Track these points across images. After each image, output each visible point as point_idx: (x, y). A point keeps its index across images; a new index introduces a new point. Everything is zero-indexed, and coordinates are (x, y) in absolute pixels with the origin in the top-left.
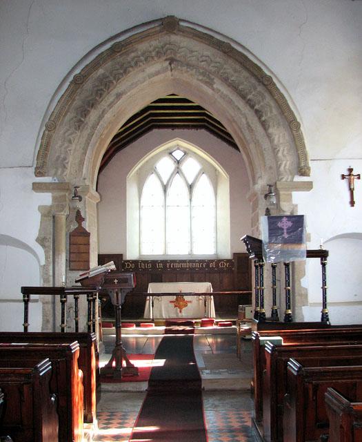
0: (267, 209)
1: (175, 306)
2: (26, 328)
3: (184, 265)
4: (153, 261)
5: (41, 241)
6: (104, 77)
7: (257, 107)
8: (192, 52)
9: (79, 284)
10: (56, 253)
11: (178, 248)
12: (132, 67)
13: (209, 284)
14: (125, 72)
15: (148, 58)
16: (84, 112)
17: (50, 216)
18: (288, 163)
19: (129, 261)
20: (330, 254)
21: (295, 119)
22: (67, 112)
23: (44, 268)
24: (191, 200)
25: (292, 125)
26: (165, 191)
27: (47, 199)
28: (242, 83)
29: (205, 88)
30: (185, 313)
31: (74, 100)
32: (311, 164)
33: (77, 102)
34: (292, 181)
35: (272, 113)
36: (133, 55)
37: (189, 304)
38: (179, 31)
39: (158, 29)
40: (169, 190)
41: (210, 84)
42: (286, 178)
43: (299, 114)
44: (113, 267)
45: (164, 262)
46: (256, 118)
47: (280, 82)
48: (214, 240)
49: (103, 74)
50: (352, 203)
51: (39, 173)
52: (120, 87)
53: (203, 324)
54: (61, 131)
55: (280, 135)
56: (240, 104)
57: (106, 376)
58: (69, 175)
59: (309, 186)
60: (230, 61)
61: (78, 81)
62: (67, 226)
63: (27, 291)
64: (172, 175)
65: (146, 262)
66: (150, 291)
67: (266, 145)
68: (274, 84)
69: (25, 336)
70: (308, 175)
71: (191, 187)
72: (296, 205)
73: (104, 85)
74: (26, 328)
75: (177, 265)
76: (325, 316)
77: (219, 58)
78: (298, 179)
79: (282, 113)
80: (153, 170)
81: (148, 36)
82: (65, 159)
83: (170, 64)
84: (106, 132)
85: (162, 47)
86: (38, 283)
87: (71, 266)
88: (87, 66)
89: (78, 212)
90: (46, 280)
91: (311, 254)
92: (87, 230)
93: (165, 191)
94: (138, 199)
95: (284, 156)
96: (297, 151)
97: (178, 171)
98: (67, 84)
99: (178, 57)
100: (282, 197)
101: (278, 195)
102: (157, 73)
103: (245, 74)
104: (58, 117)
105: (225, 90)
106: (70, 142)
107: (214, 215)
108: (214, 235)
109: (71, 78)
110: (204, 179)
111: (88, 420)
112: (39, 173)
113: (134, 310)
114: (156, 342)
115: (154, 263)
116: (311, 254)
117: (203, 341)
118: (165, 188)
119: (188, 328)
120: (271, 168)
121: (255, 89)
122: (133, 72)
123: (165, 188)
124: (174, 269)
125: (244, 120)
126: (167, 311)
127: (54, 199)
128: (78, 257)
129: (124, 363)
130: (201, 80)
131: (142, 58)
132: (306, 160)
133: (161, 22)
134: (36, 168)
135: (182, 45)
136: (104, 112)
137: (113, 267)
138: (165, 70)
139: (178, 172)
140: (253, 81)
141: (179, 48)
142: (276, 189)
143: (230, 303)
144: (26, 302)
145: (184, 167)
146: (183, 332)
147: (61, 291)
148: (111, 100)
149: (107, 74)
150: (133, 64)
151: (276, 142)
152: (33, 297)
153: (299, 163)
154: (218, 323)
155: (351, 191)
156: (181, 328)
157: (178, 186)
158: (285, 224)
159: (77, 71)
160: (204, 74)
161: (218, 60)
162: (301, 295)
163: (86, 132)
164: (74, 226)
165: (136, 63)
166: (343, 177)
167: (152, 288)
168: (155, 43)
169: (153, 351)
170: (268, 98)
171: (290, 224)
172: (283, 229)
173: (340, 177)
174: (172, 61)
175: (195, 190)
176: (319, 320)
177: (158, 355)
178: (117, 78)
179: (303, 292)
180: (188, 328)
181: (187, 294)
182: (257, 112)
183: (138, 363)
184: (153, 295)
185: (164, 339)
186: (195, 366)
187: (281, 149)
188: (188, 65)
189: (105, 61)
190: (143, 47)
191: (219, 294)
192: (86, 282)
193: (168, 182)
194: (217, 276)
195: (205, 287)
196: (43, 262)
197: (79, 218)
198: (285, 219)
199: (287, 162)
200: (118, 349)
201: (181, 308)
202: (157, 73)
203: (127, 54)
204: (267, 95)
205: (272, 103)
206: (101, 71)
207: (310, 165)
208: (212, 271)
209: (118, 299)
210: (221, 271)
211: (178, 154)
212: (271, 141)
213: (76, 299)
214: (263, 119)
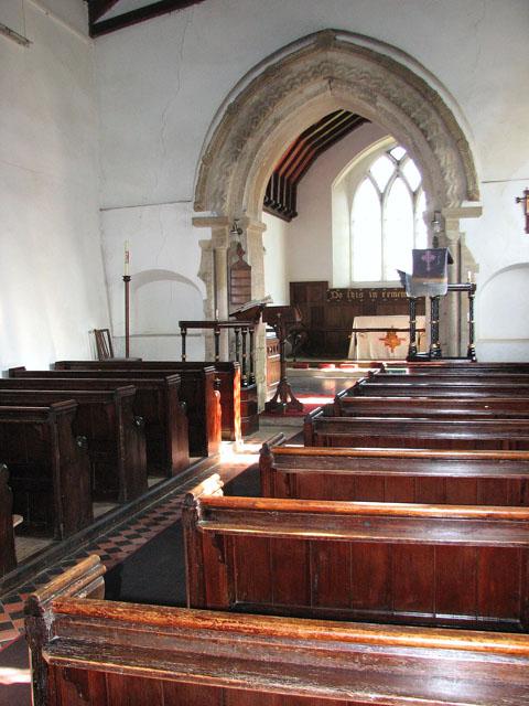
1: (386, 345)
4: (364, 290)
5: (203, 276)
7: (421, 126)
8: (350, 68)
9: (234, 318)
14: (280, 96)
15: (304, 79)
16: (240, 142)
17: (210, 250)
18: (456, 188)
19: (335, 290)
21: (463, 138)
22: (223, 143)
23: (207, 302)
27: (206, 233)
28: (405, 100)
31: (230, 130)
32: (481, 188)
33: (233, 132)
34: (459, 207)
36: (288, 77)
38: (335, 47)
39: (313, 47)
40: (388, 200)
41: (373, 102)
42: (453, 203)
45: (379, 291)
49: (259, 101)
51: (198, 208)
52: (278, 110)
54: (219, 162)
57: (272, 408)
58: (227, 208)
59: (477, 212)
60: (392, 76)
61: (233, 111)
63: (184, 325)
64: (391, 180)
65: (358, 290)
68: (440, 99)
70: (477, 200)
72: (464, 234)
73: (260, 111)
77: (379, 72)
78: (466, 204)
79: (449, 132)
80: (367, 174)
81: (303, 55)
82: (223, 192)
84: (266, 159)
85: (319, 66)
88: (241, 93)
89: (239, 245)
90: (208, 314)
92: (249, 263)
93: (382, 200)
94: (347, 212)
95: (451, 179)
96: (465, 173)
97: (398, 174)
98: (222, 113)
99: (335, 75)
100: (448, 224)
103: (408, 89)
104: (214, 150)
106: (227, 174)
109: (225, 108)
111: (229, 438)
112: (198, 208)
115: (366, 291)
118: (382, 197)
121: (420, 105)
122: (289, 95)
123: (382, 197)
124: (391, 299)
126: (376, 350)
127: (214, 233)
129: (289, 400)
130: (363, 99)
131: (297, 80)
135: (339, 62)
136: (262, 140)
138: (323, 90)
139: (398, 176)
140: (418, 96)
141: (337, 65)
144: (184, 335)
147: (215, 325)
149: (262, 100)
150: (288, 87)
151: (442, 164)
152: (190, 331)
153: (467, 187)
159: (232, 100)
160: (365, 91)
165: (293, 84)
166: (518, 200)
167: (358, 322)
170: (434, 117)
173: (514, 201)
174: (331, 79)
178: (273, 103)
182: (423, 131)
187: (449, 172)
188: (349, 82)
190: (297, 67)
193: (385, 191)
196: (205, 297)
204: (433, 111)
205: (439, 122)
206: (256, 98)
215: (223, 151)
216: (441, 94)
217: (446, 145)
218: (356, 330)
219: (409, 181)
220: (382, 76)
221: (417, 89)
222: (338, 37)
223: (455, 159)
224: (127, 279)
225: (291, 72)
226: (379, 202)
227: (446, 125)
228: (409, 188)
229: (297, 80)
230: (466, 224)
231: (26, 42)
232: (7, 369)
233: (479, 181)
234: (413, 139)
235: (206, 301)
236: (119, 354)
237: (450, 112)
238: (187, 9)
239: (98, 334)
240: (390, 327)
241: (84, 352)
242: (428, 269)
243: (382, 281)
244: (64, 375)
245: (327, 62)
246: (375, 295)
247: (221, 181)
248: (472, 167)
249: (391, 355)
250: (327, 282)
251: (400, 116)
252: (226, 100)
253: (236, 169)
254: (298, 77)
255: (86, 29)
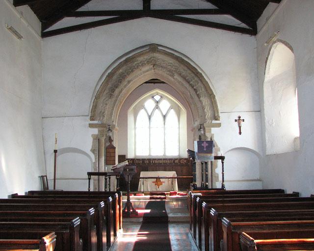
0: (200, 136)
2: (89, 190)
3: (160, 162)
4: (142, 159)
5: (93, 151)
6: (123, 73)
7: (195, 87)
10: (100, 157)
11: (157, 152)
12: (135, 68)
13: (174, 172)
14: (132, 71)
15: (143, 64)
16: (113, 90)
17: (97, 139)
20: (225, 158)
21: (213, 94)
24: (164, 124)
25: (211, 96)
26: (150, 119)
27: (95, 131)
29: (170, 78)
30: (161, 189)
32: (220, 115)
33: (110, 86)
35: (202, 91)
36: (136, 63)
37: (163, 184)
38: (158, 51)
39: (148, 50)
40: (152, 118)
41: (173, 76)
42: (208, 121)
43: (214, 88)
44: (127, 163)
45: (149, 160)
46: (194, 92)
47: (206, 75)
48: (178, 147)
50: (240, 133)
51: (92, 119)
52: (129, 78)
53: (171, 194)
54: (101, 100)
55: (205, 101)
56: (187, 85)
58: (105, 120)
59: (219, 125)
60: (182, 66)
61: (110, 76)
62: (105, 144)
63: (90, 174)
64: (154, 110)
66: (141, 176)
67: (199, 105)
69: (89, 193)
71: (164, 117)
73: (123, 77)
74: (89, 190)
75: (156, 162)
76: (223, 186)
77: (177, 64)
78: (214, 122)
80: (143, 107)
82: (104, 112)
83: (153, 66)
85: (150, 59)
86: (48, 178)
87: (107, 163)
89: (110, 137)
90: (94, 169)
91: (217, 158)
93: (150, 119)
97: (157, 107)
99: (157, 63)
101: (204, 129)
102: (148, 71)
103: (189, 71)
104: (101, 93)
105: (180, 79)
106: (106, 104)
107: (178, 132)
108: (178, 144)
109: (107, 74)
110: (172, 112)
113: (133, 188)
114: (145, 204)
115: (143, 160)
116: (217, 158)
117: (171, 203)
118: (150, 117)
119: (163, 196)
120: (201, 116)
121: (194, 79)
123: (150, 117)
125: (189, 93)
126: (151, 187)
127: (99, 131)
128: (109, 160)
131: (140, 64)
132: (218, 112)
133: (149, 47)
134: (91, 117)
137: (127, 163)
139: (157, 108)
140: (193, 75)
142: (204, 127)
143: (185, 183)
144: (89, 179)
145: (160, 105)
146: (160, 198)
148: (125, 84)
150: (136, 67)
151: (204, 104)
152: (92, 177)
153: (215, 114)
154: (179, 194)
155: (240, 127)
156: (159, 196)
157: (157, 116)
158: (205, 145)
159: (110, 71)
161: (176, 65)
162: (215, 177)
163: (114, 99)
164: (108, 144)
165: (138, 66)
166: (236, 121)
167: (143, 174)
168: (146, 57)
169: (144, 206)
170: (200, 84)
171: (207, 145)
172: (204, 147)
173: (234, 121)
175: (167, 118)
176: (221, 188)
177: (146, 208)
179: (217, 175)
180: (163, 196)
181: (162, 178)
182: (195, 89)
183: (139, 211)
184: (143, 178)
185: (149, 202)
186: (166, 212)
189: (123, 66)
190: (141, 59)
191: (179, 178)
192: (116, 170)
194: (179, 168)
195: (172, 174)
196: (94, 161)
197: (110, 140)
198: (205, 143)
199: (209, 114)
200: (128, 204)
201: (159, 186)
202: (148, 71)
203: (133, 62)
206: (121, 71)
207: (220, 115)
208: (176, 165)
209: (128, 179)
210: (182, 165)
211: (157, 98)
212: (202, 103)
213: (110, 178)
214: (198, 93)
215: (105, 93)
216: (203, 74)
217: (205, 96)
218: (141, 178)
219: (162, 111)
220: (177, 65)
221: (193, 72)
222: (159, 48)
223: (209, 102)
224: (55, 151)
225: (138, 60)
226: (148, 119)
227: (205, 88)
228: (162, 114)
229: (140, 64)
230: (214, 130)
231: (20, 37)
232: (11, 194)
233: (220, 112)
234: (190, 92)
235: (94, 163)
236: (51, 188)
237: (207, 83)
238: (88, 29)
239: (42, 177)
240: (157, 176)
241: (36, 187)
242: (205, 150)
243: (150, 155)
244: (30, 197)
245: (153, 57)
246: (147, 162)
247: (103, 107)
248: (217, 106)
249: (158, 189)
250: (125, 156)
251: (184, 83)
252: (106, 71)
253: (110, 102)
254: (140, 63)
255: (40, 35)
